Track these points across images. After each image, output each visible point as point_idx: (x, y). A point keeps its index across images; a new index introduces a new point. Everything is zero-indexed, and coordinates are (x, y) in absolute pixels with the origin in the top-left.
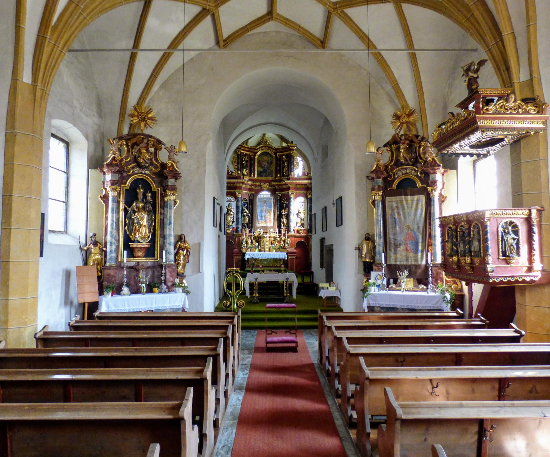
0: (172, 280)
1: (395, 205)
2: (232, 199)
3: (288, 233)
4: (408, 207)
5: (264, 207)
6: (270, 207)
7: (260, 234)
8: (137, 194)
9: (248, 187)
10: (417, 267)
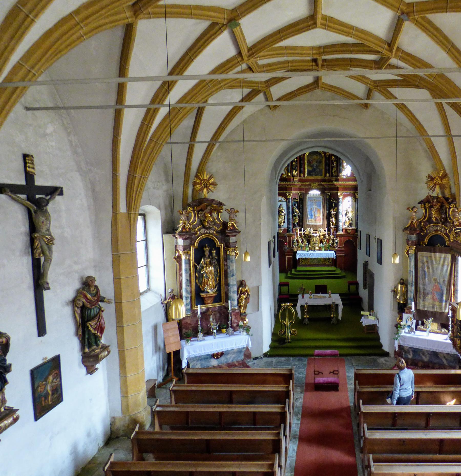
0: (236, 321)
1: (425, 260)
2: (283, 199)
3: (336, 233)
4: (436, 263)
5: (314, 207)
6: (320, 206)
7: (310, 233)
8: (204, 252)
9: (298, 186)
10: (441, 313)
